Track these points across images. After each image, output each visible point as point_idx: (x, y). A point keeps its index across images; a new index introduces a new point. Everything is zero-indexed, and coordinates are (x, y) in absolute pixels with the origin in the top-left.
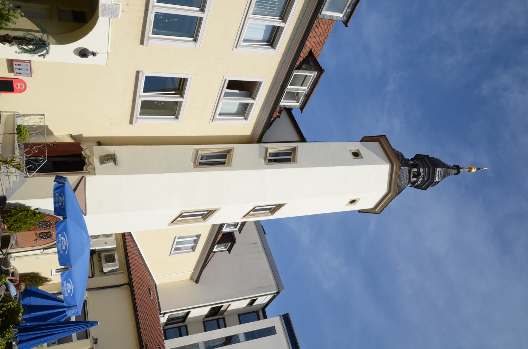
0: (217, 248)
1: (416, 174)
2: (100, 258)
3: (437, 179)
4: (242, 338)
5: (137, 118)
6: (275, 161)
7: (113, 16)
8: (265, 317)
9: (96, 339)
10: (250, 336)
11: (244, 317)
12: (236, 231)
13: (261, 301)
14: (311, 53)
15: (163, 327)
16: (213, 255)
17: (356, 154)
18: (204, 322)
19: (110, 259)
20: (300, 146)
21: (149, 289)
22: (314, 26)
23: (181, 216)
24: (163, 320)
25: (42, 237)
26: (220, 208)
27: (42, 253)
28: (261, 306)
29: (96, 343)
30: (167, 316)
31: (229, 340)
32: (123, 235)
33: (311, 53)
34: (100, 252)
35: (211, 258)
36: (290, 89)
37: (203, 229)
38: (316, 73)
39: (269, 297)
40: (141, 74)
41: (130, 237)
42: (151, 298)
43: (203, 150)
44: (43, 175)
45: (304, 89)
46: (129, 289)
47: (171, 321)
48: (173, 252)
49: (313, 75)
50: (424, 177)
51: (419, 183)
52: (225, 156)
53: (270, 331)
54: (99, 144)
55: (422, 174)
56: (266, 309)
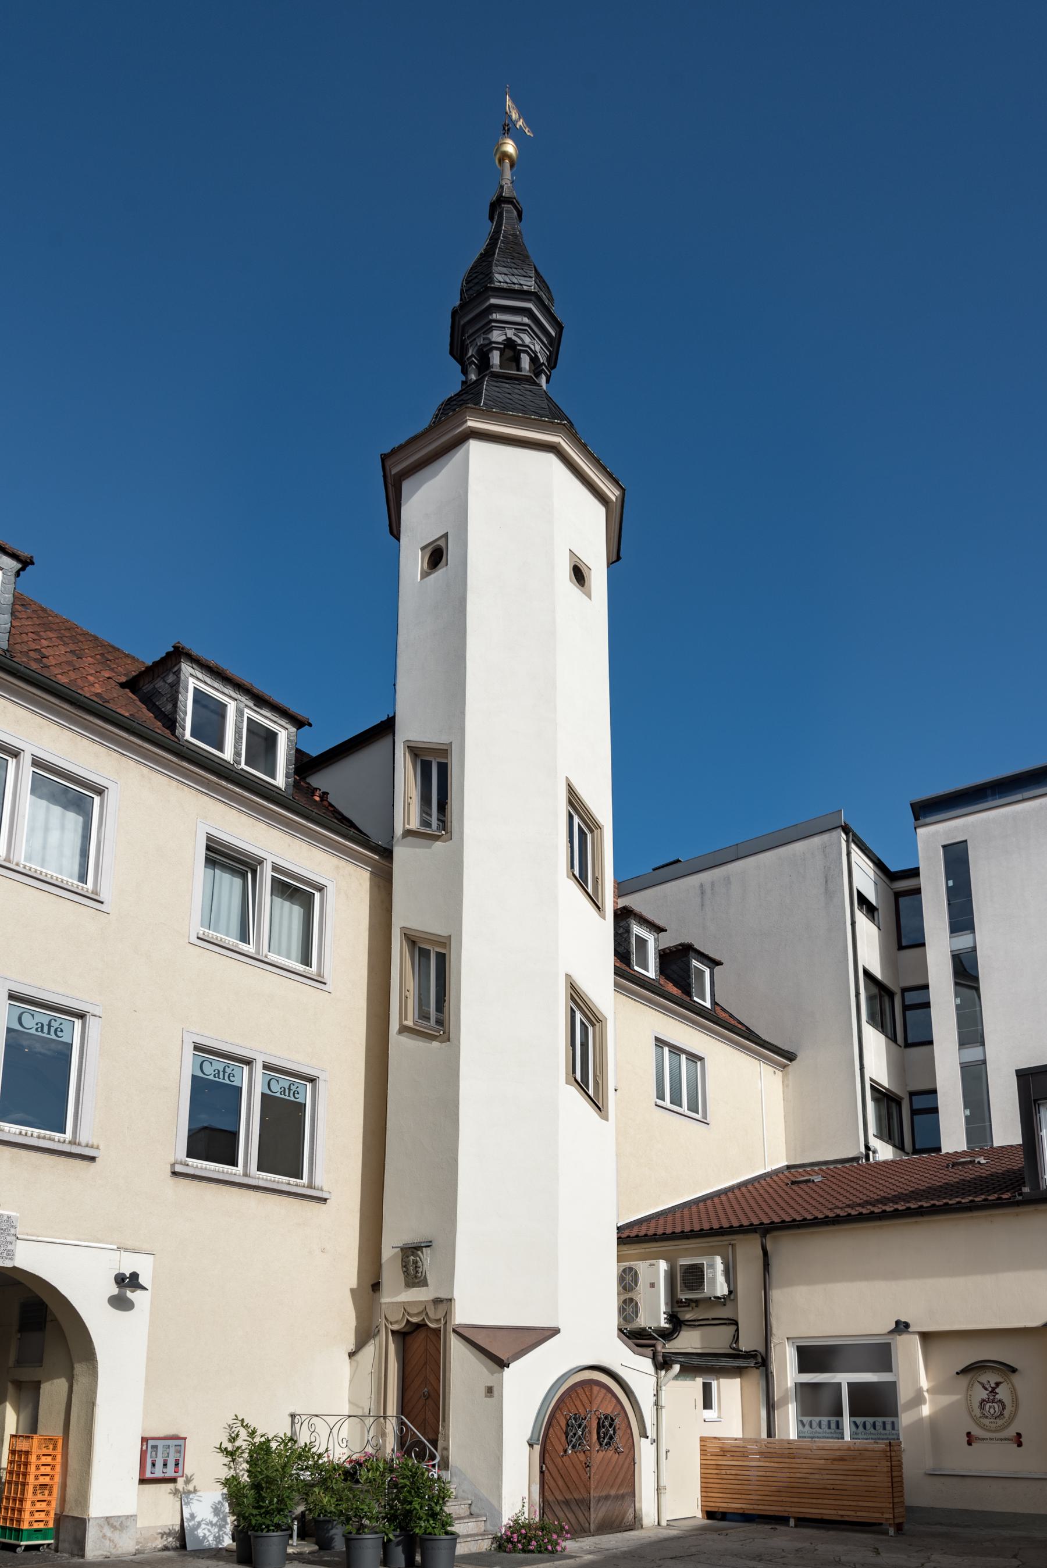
0: (646, 969)
1: (509, 353)
2: (689, 1301)
3: (530, 284)
4: (963, 941)
5: (310, 1186)
6: (443, 807)
7: (13, 1231)
8: (915, 873)
9: (898, 1323)
10: (961, 919)
11: (905, 938)
12: (656, 940)
13: (865, 878)
14: (132, 685)
15: (907, 1154)
16: (723, 1010)
17: (436, 557)
18: (907, 1045)
19: (694, 1276)
20: (407, 731)
21: (793, 1183)
22: (34, 666)
23: (582, 1085)
24: (884, 1152)
25: (611, 1438)
26: (568, 976)
27: (656, 1441)
28: (879, 882)
29: (907, 1325)
30: (875, 1143)
31: (966, 972)
32: (622, 1241)
33: (132, 685)
34: (673, 1301)
35: (731, 1016)
36: (237, 754)
37: (635, 1029)
38: (186, 668)
39: (858, 857)
40: (179, 1168)
41: (645, 1224)
42: (818, 1179)
43: (403, 1015)
44: (446, 1427)
45: (237, 713)
46: (775, 1233)
47: (889, 1132)
48: (699, 1117)
49: (191, 680)
50: (520, 328)
51: (538, 348)
52: (424, 954)
53: (957, 859)
54: (376, 1287)
55: (510, 333)
56: (893, 868)
